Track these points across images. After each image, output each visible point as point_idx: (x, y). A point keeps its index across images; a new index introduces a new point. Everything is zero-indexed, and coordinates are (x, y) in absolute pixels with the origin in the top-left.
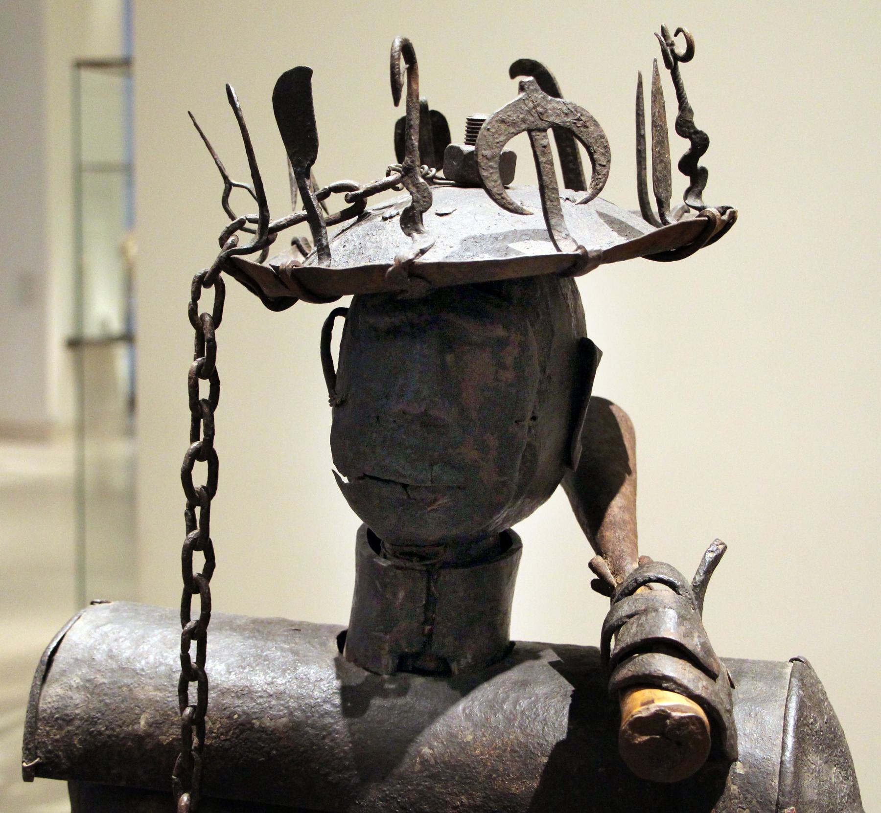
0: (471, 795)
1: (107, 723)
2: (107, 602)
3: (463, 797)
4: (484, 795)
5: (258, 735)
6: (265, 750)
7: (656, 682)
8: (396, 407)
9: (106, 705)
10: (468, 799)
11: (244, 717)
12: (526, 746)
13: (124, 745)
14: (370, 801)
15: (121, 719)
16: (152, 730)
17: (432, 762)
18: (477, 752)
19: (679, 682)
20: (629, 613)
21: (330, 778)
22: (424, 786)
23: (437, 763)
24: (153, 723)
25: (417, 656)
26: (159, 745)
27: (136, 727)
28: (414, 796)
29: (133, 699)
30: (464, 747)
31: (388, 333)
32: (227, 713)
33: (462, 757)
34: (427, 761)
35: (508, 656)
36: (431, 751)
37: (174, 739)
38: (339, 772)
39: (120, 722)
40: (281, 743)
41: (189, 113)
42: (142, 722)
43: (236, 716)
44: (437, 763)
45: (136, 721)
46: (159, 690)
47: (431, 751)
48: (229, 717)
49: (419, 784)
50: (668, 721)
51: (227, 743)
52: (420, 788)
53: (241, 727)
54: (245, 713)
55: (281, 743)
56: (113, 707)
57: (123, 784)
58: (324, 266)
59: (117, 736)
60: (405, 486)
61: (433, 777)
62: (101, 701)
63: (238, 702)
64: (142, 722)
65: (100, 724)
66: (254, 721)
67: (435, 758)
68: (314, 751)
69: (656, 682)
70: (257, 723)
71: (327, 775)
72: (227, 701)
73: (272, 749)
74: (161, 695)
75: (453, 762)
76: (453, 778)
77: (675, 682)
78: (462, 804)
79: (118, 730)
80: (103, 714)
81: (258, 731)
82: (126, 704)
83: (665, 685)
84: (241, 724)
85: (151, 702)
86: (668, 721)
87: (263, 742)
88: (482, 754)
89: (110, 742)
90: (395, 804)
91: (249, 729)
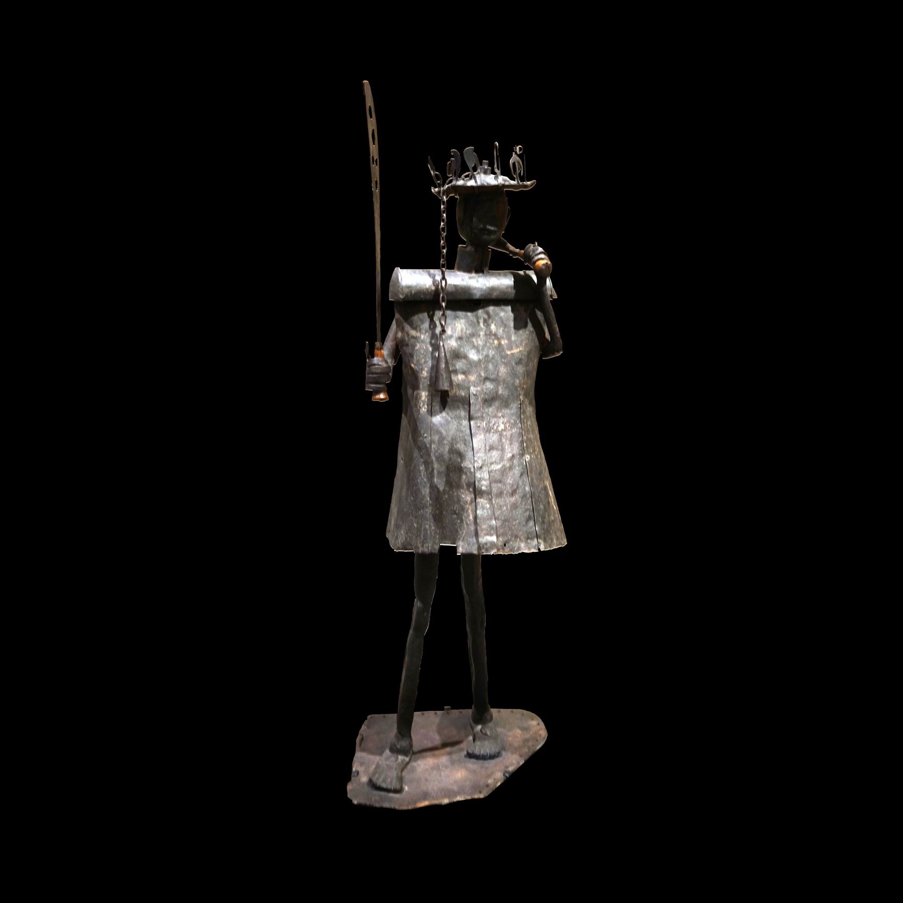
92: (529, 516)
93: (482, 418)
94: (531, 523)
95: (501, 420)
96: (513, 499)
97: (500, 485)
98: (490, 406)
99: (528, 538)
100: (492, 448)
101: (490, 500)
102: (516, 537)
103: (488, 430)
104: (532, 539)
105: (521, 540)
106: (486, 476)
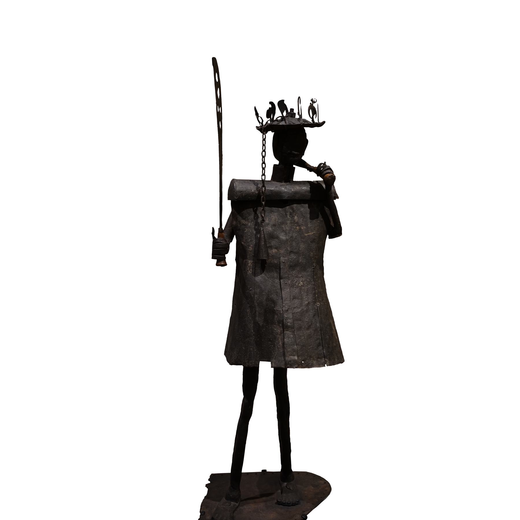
41: (214, 60)
92: (319, 343)
93: (288, 278)
94: (321, 348)
95: (301, 279)
96: (308, 332)
97: (300, 322)
98: (294, 270)
99: (318, 358)
100: (294, 298)
101: (293, 332)
102: (311, 357)
103: (292, 286)
104: (321, 358)
105: (314, 359)
106: (291, 316)
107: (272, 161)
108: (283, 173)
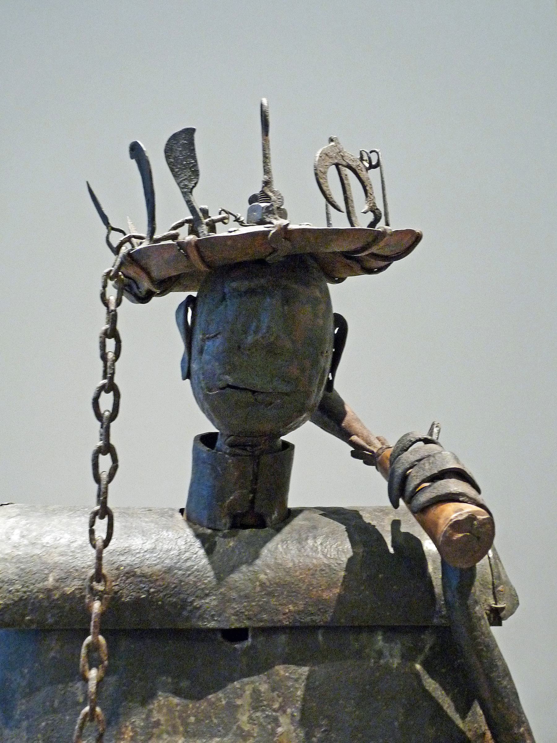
0: (296, 603)
1: (23, 583)
2: (12, 504)
3: (290, 606)
4: (305, 602)
5: (140, 579)
6: (145, 589)
7: (453, 498)
8: (250, 339)
9: (22, 570)
10: (294, 607)
11: (128, 568)
12: (329, 566)
13: (37, 597)
14: (226, 617)
15: (34, 579)
16: (57, 584)
17: (268, 584)
18: (298, 573)
19: (470, 496)
20: (418, 458)
21: (195, 604)
22: (264, 601)
23: (271, 584)
24: (59, 579)
25: (243, 515)
26: (64, 595)
27: (46, 583)
28: (256, 609)
29: (42, 563)
30: (288, 571)
31: (246, 292)
32: (115, 566)
33: (288, 579)
34: (264, 583)
35: (290, 515)
36: (266, 577)
37: (76, 589)
38: (202, 598)
39: (33, 581)
40: (158, 583)
42: (51, 579)
43: (122, 568)
44: (271, 584)
45: (45, 579)
46: (62, 555)
47: (266, 577)
48: (117, 569)
49: (258, 601)
50: (475, 522)
51: (117, 587)
52: (261, 603)
53: (127, 575)
54: (128, 565)
55: (158, 583)
56: (28, 570)
57: (34, 627)
58: (213, 235)
59: (30, 591)
60: (254, 392)
61: (270, 594)
62: (18, 568)
63: (122, 558)
64: (51, 579)
65: (18, 584)
66: (136, 570)
67: (269, 581)
68: (182, 586)
69: (453, 498)
70: (138, 571)
71: (191, 603)
72: (115, 558)
73: (151, 588)
74: (64, 558)
75: (282, 582)
76: (282, 593)
77: (468, 497)
78: (290, 611)
79: (31, 587)
80: (20, 577)
81: (140, 576)
82: (38, 567)
83: (461, 499)
84: (127, 573)
85: (56, 565)
86: (475, 522)
87: (144, 584)
88: (301, 574)
89: (26, 597)
90: (244, 617)
91: (133, 576)
107: (168, 422)
108: (242, 489)
